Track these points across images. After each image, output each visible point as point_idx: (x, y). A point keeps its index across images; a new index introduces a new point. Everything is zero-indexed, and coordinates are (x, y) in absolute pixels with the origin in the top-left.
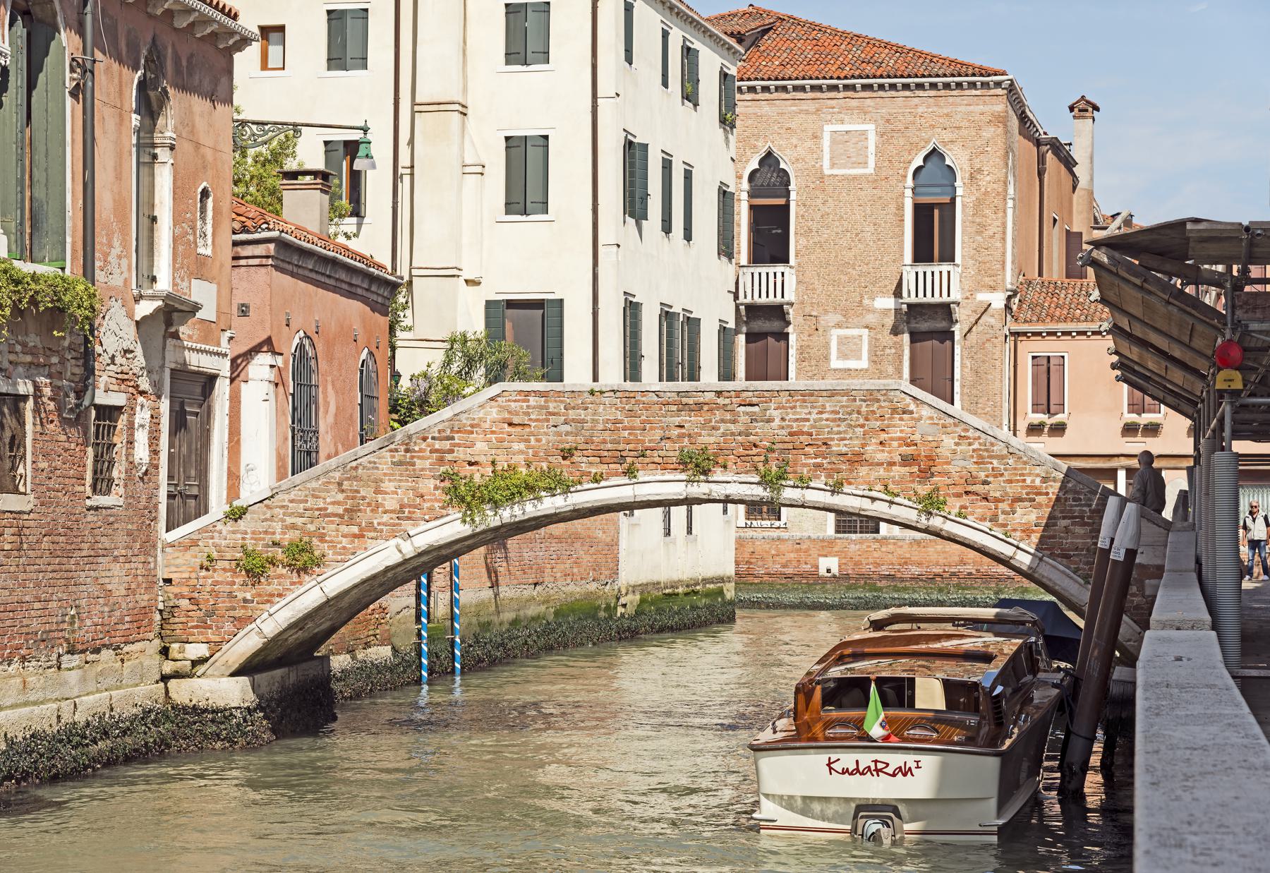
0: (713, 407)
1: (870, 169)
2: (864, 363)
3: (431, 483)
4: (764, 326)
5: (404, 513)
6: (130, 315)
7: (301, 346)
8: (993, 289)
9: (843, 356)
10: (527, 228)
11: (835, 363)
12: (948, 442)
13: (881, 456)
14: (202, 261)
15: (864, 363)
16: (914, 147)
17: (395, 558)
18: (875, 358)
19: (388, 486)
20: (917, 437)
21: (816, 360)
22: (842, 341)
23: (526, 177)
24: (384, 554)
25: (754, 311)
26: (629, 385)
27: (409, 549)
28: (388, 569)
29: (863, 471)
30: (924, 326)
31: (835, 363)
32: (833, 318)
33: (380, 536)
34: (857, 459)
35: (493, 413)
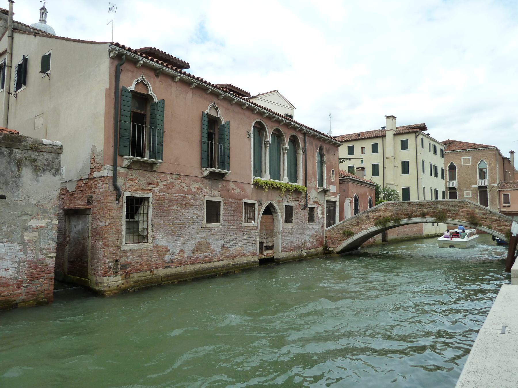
0: (426, 205)
1: (470, 164)
2: (471, 196)
3: (372, 220)
4: (452, 192)
5: (368, 225)
6: (317, 191)
7: (356, 196)
8: (495, 183)
9: (467, 195)
10: (406, 176)
11: (465, 197)
12: (477, 211)
13: (462, 214)
14: (332, 182)
15: (471, 196)
16: (478, 160)
17: (366, 233)
18: (473, 195)
19: (364, 220)
20: (470, 210)
21: (462, 196)
22: (467, 193)
23: (405, 168)
24: (364, 233)
25: (450, 188)
26: (444, 200)
27: (368, 232)
28: (365, 235)
29: (458, 217)
30: (482, 190)
31: (465, 197)
32: (464, 189)
33: (363, 229)
34: (457, 214)
35: (383, 207)
